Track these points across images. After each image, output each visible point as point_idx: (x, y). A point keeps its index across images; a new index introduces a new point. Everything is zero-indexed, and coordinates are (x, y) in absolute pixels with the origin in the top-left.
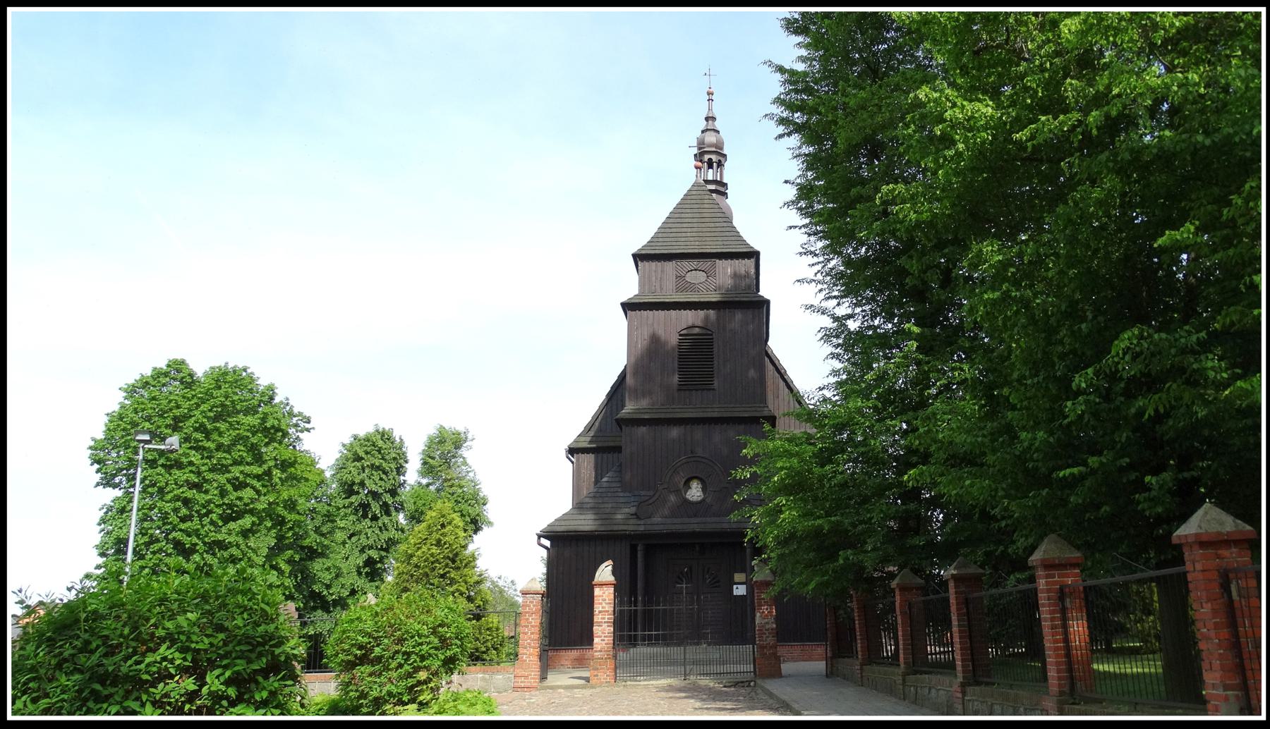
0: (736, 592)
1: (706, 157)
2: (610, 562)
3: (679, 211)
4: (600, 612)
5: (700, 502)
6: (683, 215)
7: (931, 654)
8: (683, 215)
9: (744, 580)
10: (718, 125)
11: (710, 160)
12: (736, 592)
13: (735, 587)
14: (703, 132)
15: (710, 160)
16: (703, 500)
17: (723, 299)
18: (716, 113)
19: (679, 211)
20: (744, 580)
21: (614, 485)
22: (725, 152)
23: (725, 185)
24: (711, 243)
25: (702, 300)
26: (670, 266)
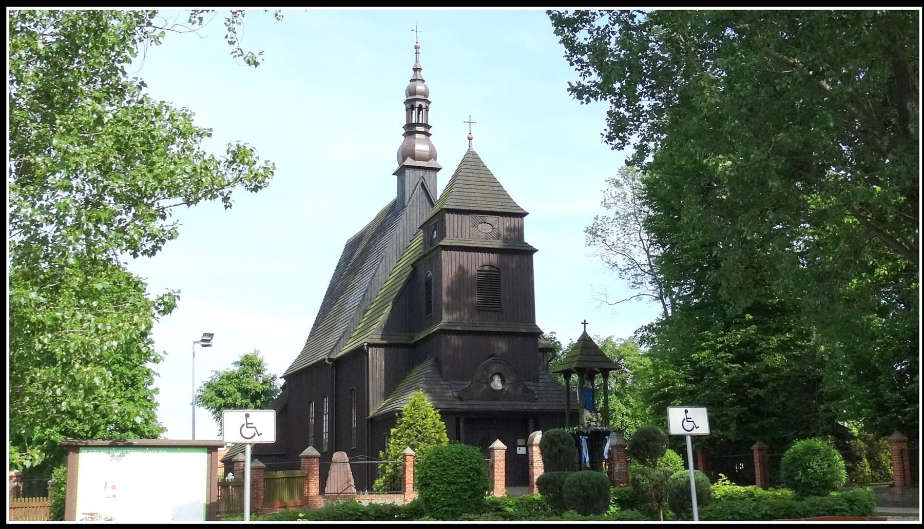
0: (519, 452)
1: (418, 103)
2: (541, 432)
4: (537, 461)
5: (500, 391)
6: (469, 178)
8: (469, 178)
10: (423, 74)
11: (420, 106)
12: (519, 452)
13: (518, 448)
14: (412, 81)
15: (420, 106)
16: (503, 389)
17: (504, 247)
18: (421, 64)
20: (524, 444)
21: (434, 375)
22: (429, 99)
23: (429, 127)
24: (494, 203)
25: (494, 247)
26: (467, 218)
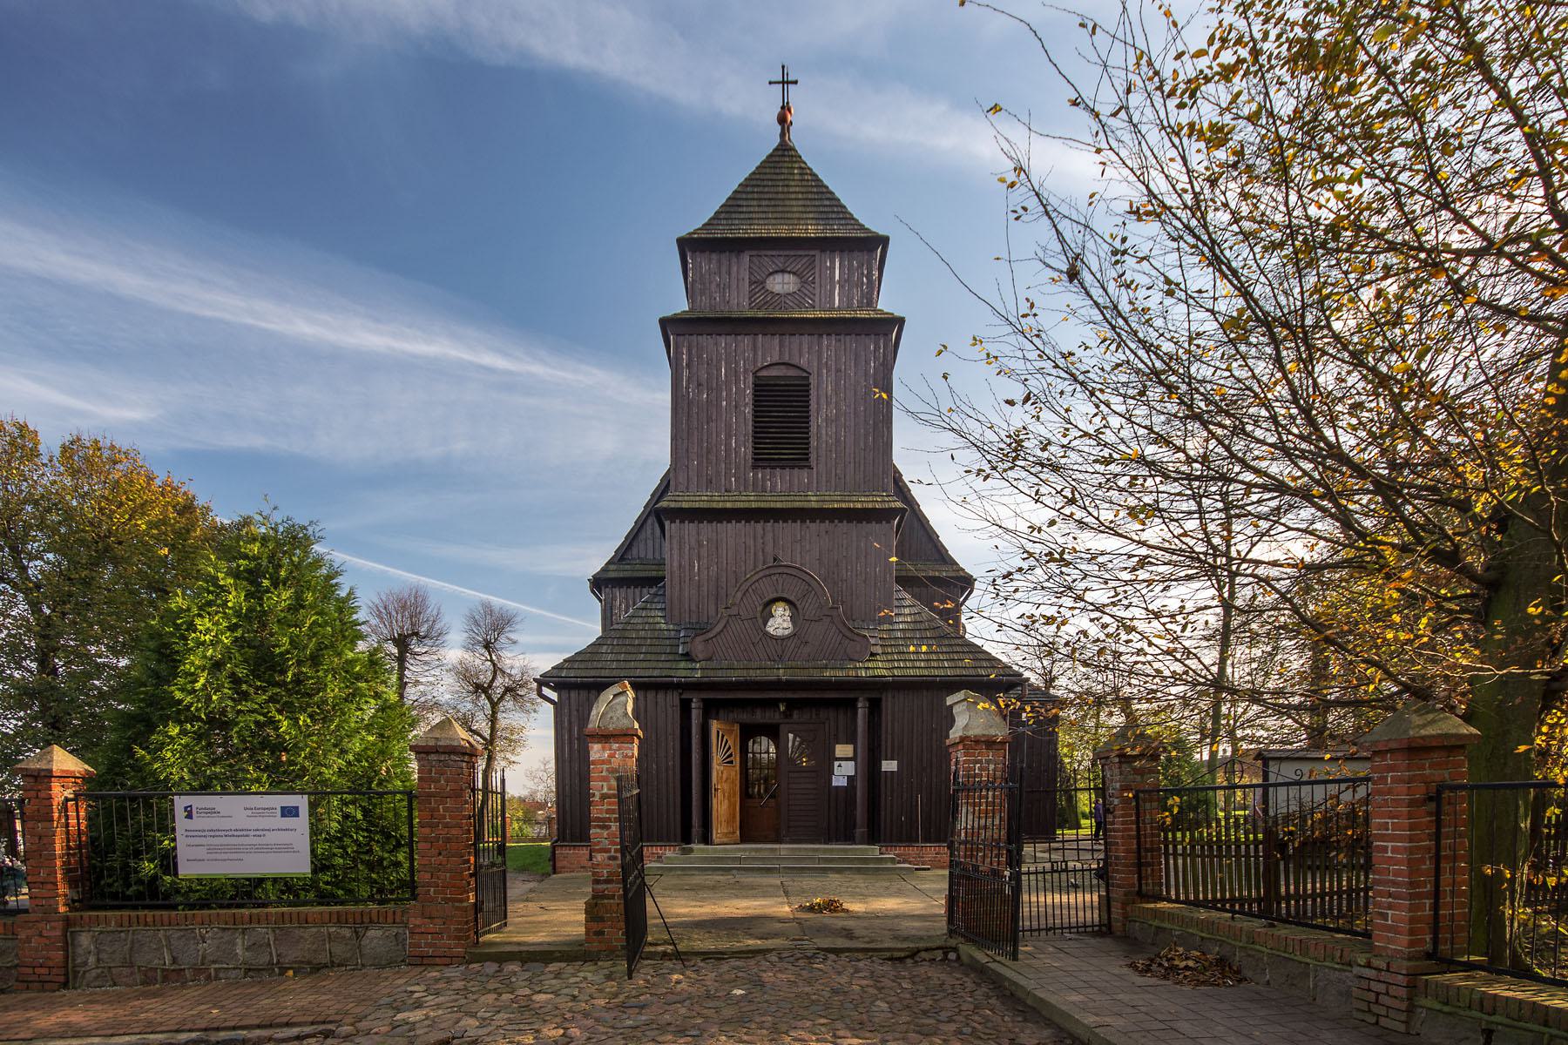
3: (728, 209)
7: (1288, 897)
9: (851, 755)
13: (836, 763)
19: (728, 209)
20: (851, 755)
